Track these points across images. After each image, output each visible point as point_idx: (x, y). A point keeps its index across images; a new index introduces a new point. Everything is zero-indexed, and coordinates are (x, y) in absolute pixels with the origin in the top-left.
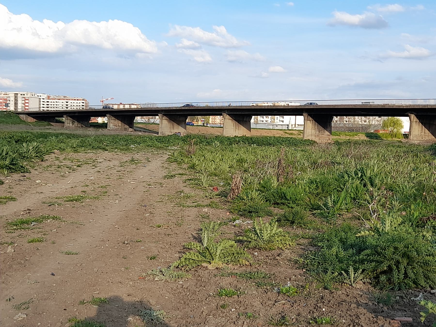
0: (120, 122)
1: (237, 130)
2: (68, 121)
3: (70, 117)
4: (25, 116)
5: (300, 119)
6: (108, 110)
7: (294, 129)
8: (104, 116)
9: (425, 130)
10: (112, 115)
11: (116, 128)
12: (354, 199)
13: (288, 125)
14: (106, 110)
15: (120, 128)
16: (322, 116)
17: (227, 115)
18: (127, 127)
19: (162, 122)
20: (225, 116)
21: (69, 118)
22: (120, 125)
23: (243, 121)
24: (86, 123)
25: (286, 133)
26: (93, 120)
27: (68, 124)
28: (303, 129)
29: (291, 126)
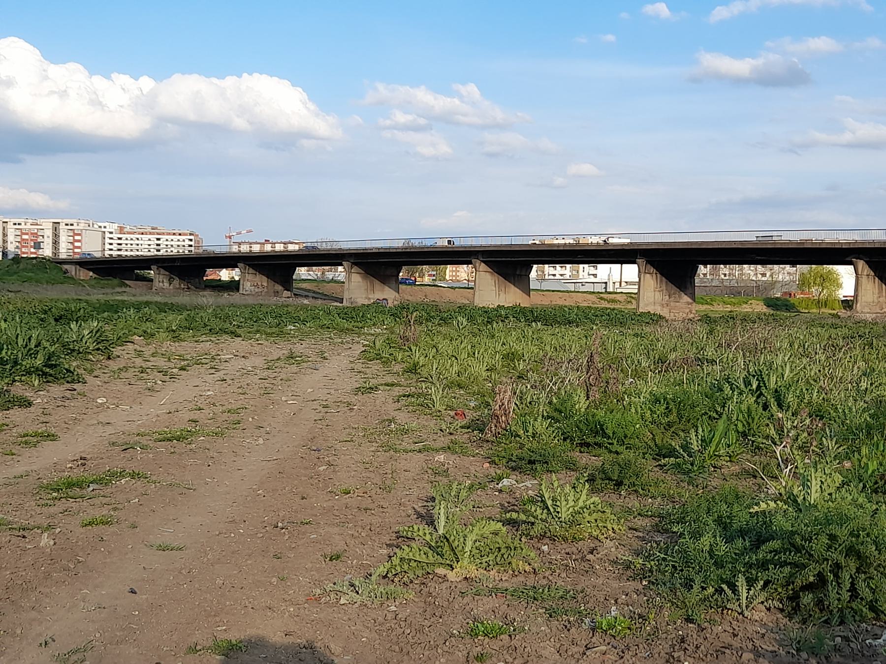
0: (265, 278)
1: (502, 294)
2: (161, 277)
4: (73, 267)
5: (631, 271)
7: (619, 291)
10: (249, 265)
11: (257, 290)
13: (606, 283)
17: (483, 264)
18: (279, 288)
19: (349, 278)
21: (355, 269)
22: (265, 284)
25: (601, 298)
27: (161, 284)
28: (636, 291)
29: (611, 284)
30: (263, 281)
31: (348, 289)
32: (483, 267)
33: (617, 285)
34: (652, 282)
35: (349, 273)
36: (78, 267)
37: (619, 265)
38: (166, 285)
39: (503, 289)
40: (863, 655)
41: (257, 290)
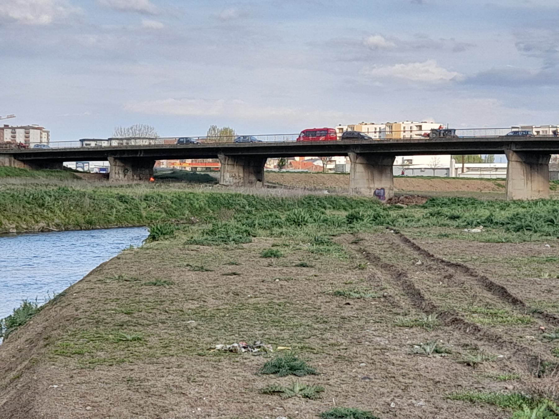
0: (241, 170)
1: (529, 183)
2: (117, 168)
3: (122, 160)
5: (500, 162)
7: (461, 176)
11: (235, 181)
13: (448, 169)
14: (182, 147)
15: (242, 181)
17: (515, 154)
18: (253, 178)
19: (354, 169)
20: (510, 155)
21: (118, 163)
22: (241, 175)
23: (537, 164)
24: (147, 171)
25: (499, 185)
27: (117, 176)
28: (505, 177)
30: (238, 171)
32: (514, 157)
34: (518, 169)
35: (353, 163)
36: (13, 159)
37: (461, 156)
41: (235, 181)
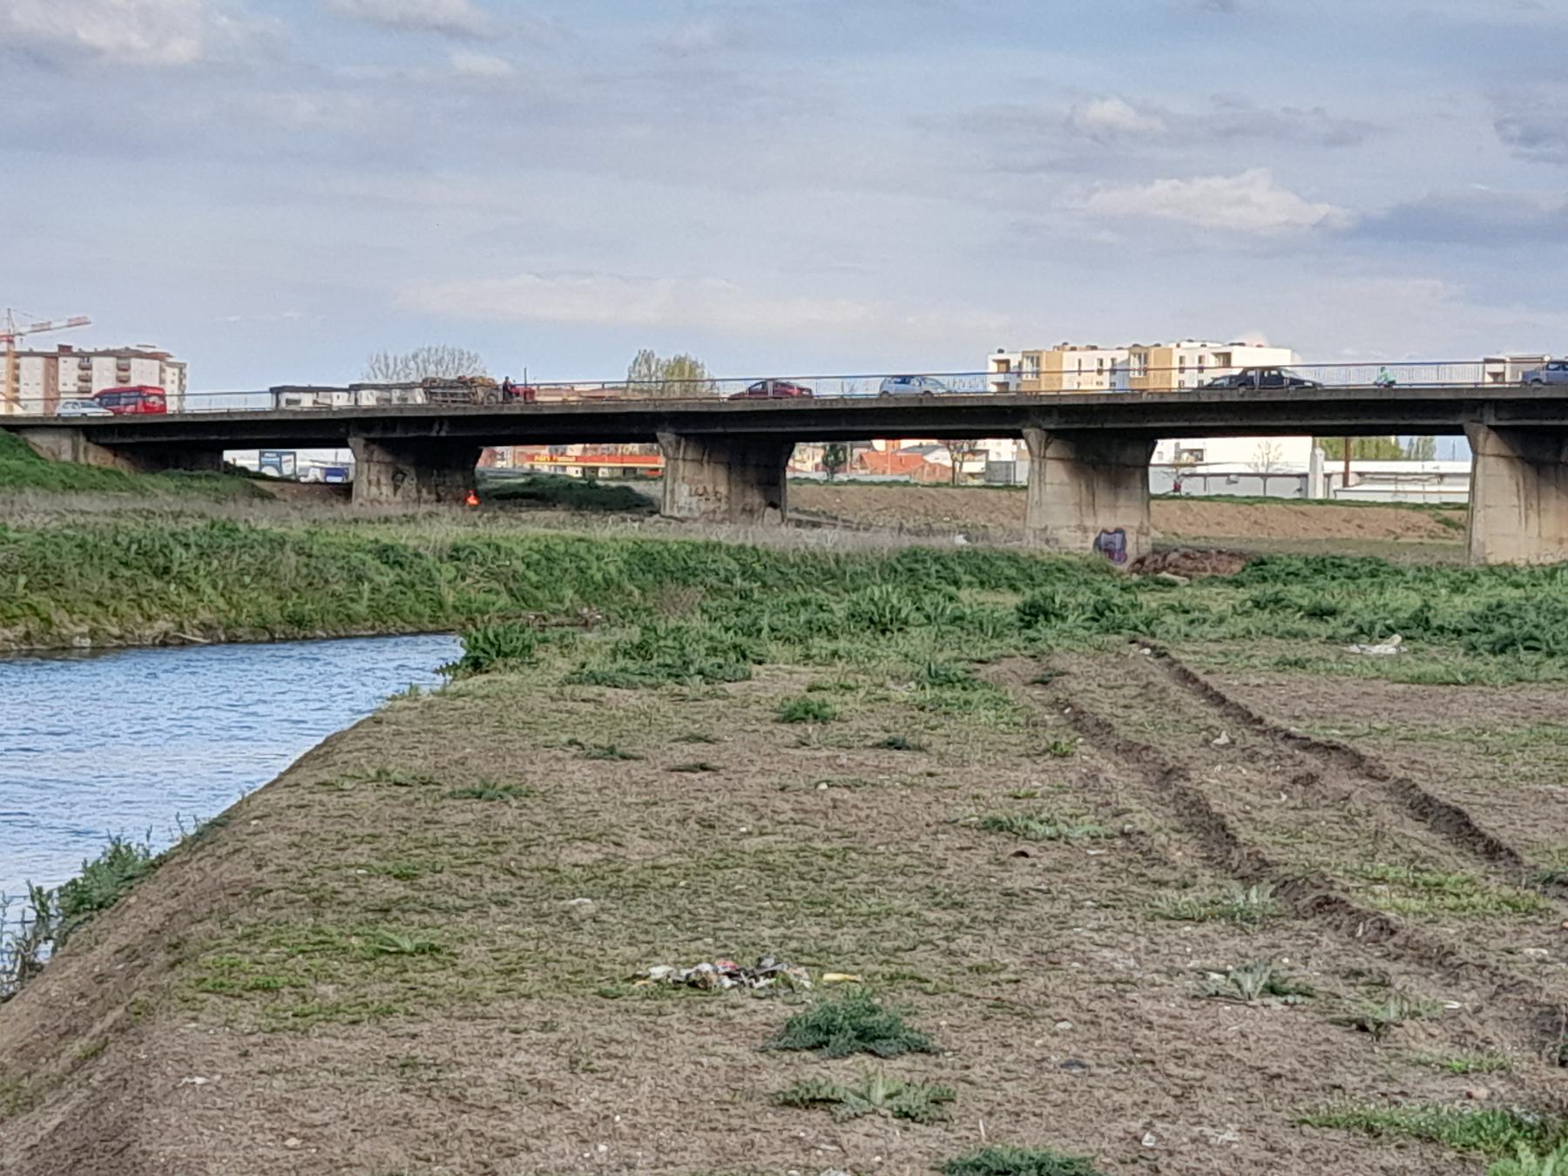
0: (721, 474)
1: (1533, 516)
2: (375, 469)
3: (384, 444)
4: (66, 443)
5: (1451, 456)
6: (1278, 396)
7: (1341, 496)
8: (341, 443)
9: (86, 450)
10: (686, 436)
11: (703, 506)
12: (359, 578)
13: (1305, 476)
16: (1106, 436)
17: (1493, 436)
18: (755, 499)
19: (1039, 474)
20: (1481, 437)
22: (723, 490)
25: (1448, 523)
26: (504, 462)
27: (374, 490)
28: (1464, 499)
29: (1320, 478)
30: (715, 479)
31: (1040, 504)
32: (1491, 444)
33: (1337, 483)
34: (1502, 479)
35: (1038, 458)
36: (82, 440)
38: (387, 490)
39: (1535, 503)
40: (618, 785)
